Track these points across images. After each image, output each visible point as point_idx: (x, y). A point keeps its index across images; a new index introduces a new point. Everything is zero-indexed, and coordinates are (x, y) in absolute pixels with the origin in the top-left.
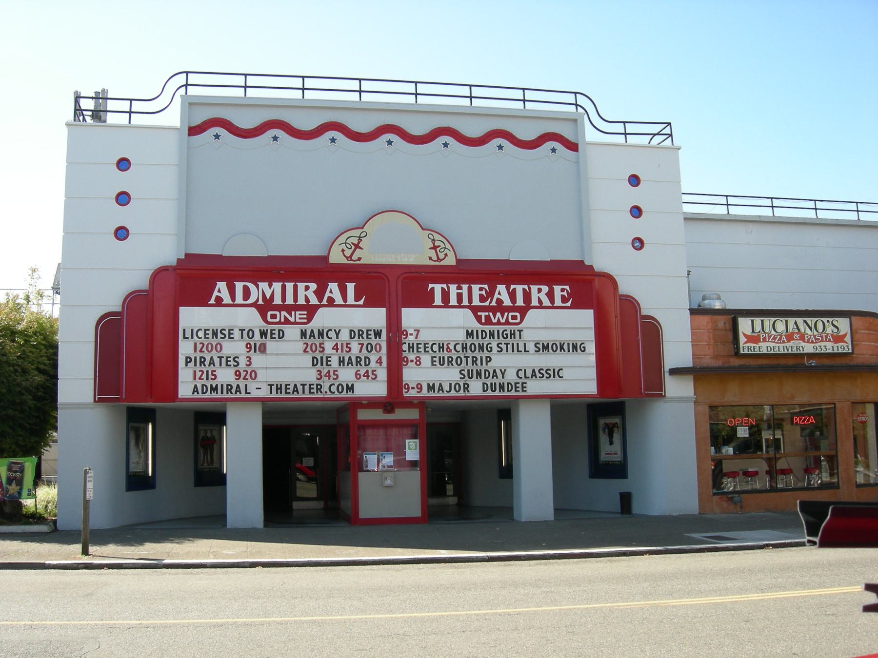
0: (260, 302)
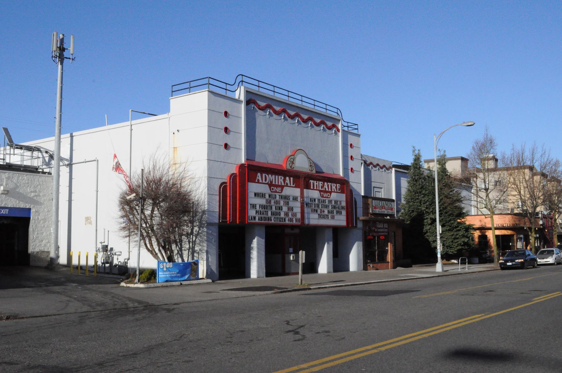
0: (269, 183)
